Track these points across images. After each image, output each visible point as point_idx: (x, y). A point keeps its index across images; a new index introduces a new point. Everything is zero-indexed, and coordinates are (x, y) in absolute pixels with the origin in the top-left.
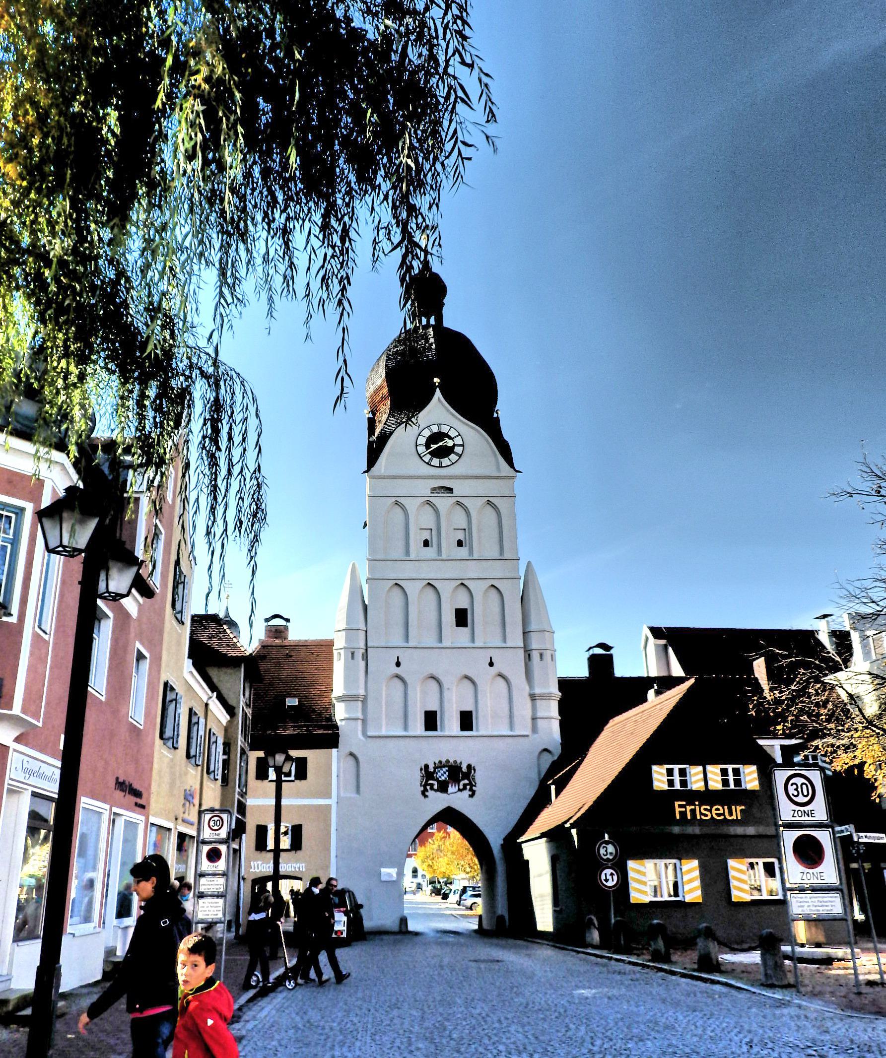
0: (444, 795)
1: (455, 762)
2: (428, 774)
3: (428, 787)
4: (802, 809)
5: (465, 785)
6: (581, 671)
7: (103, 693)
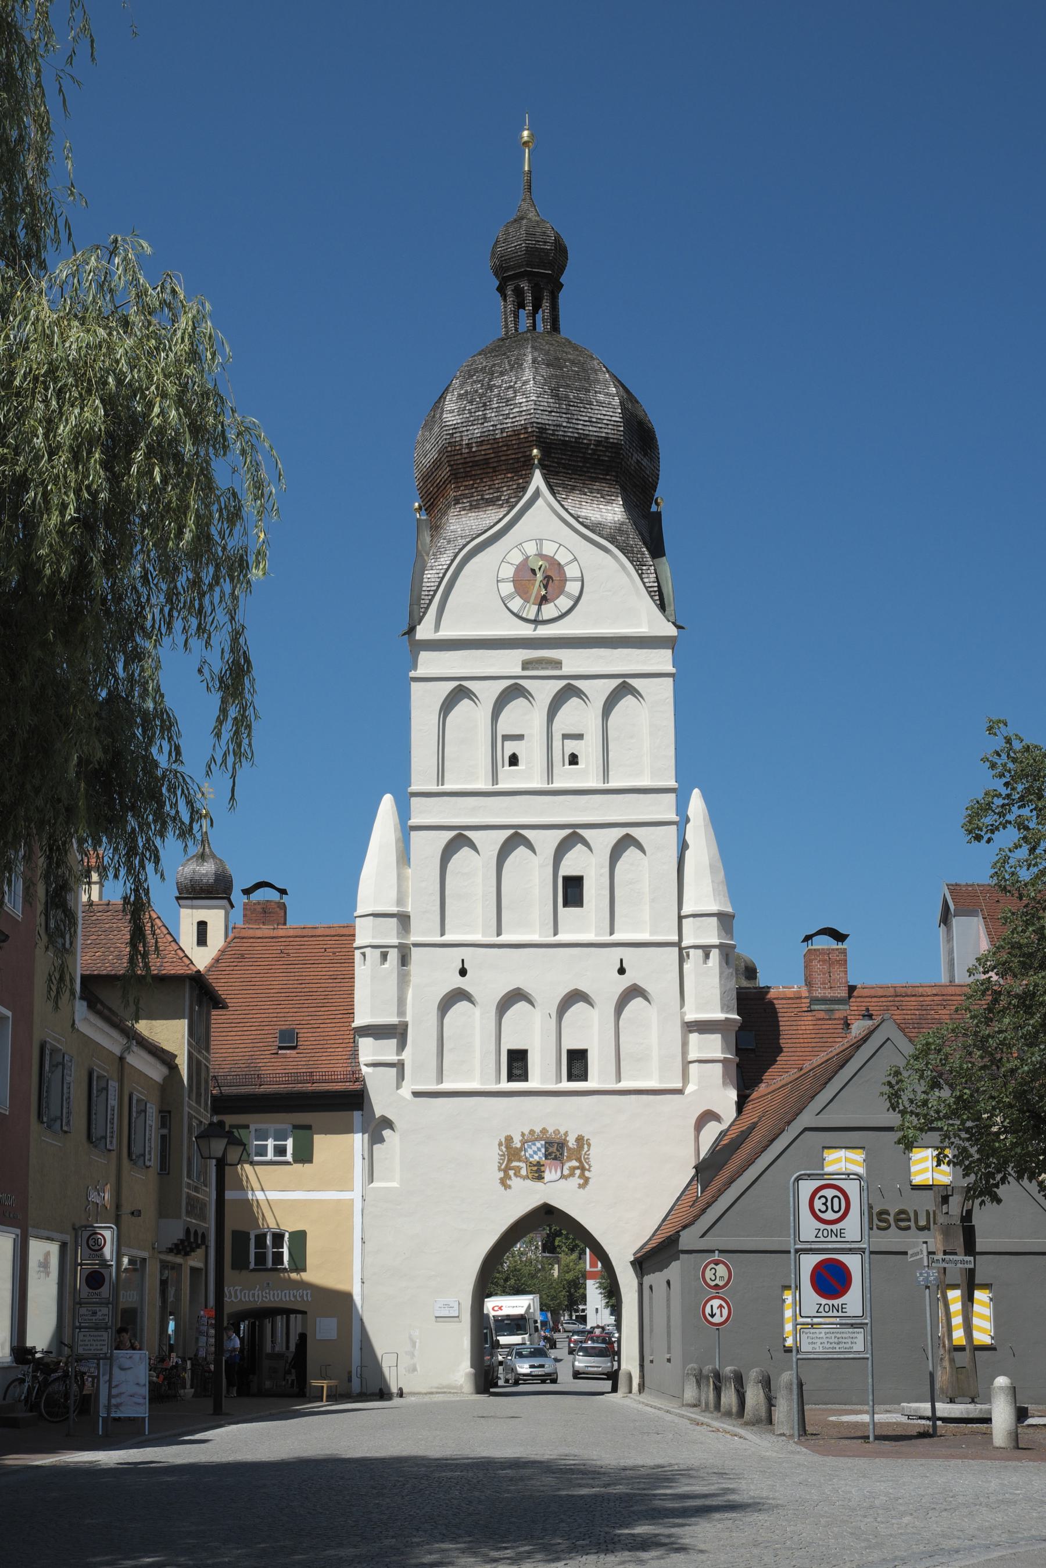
0: (539, 1185)
2: (511, 1153)
3: (511, 1173)
4: (829, 1227)
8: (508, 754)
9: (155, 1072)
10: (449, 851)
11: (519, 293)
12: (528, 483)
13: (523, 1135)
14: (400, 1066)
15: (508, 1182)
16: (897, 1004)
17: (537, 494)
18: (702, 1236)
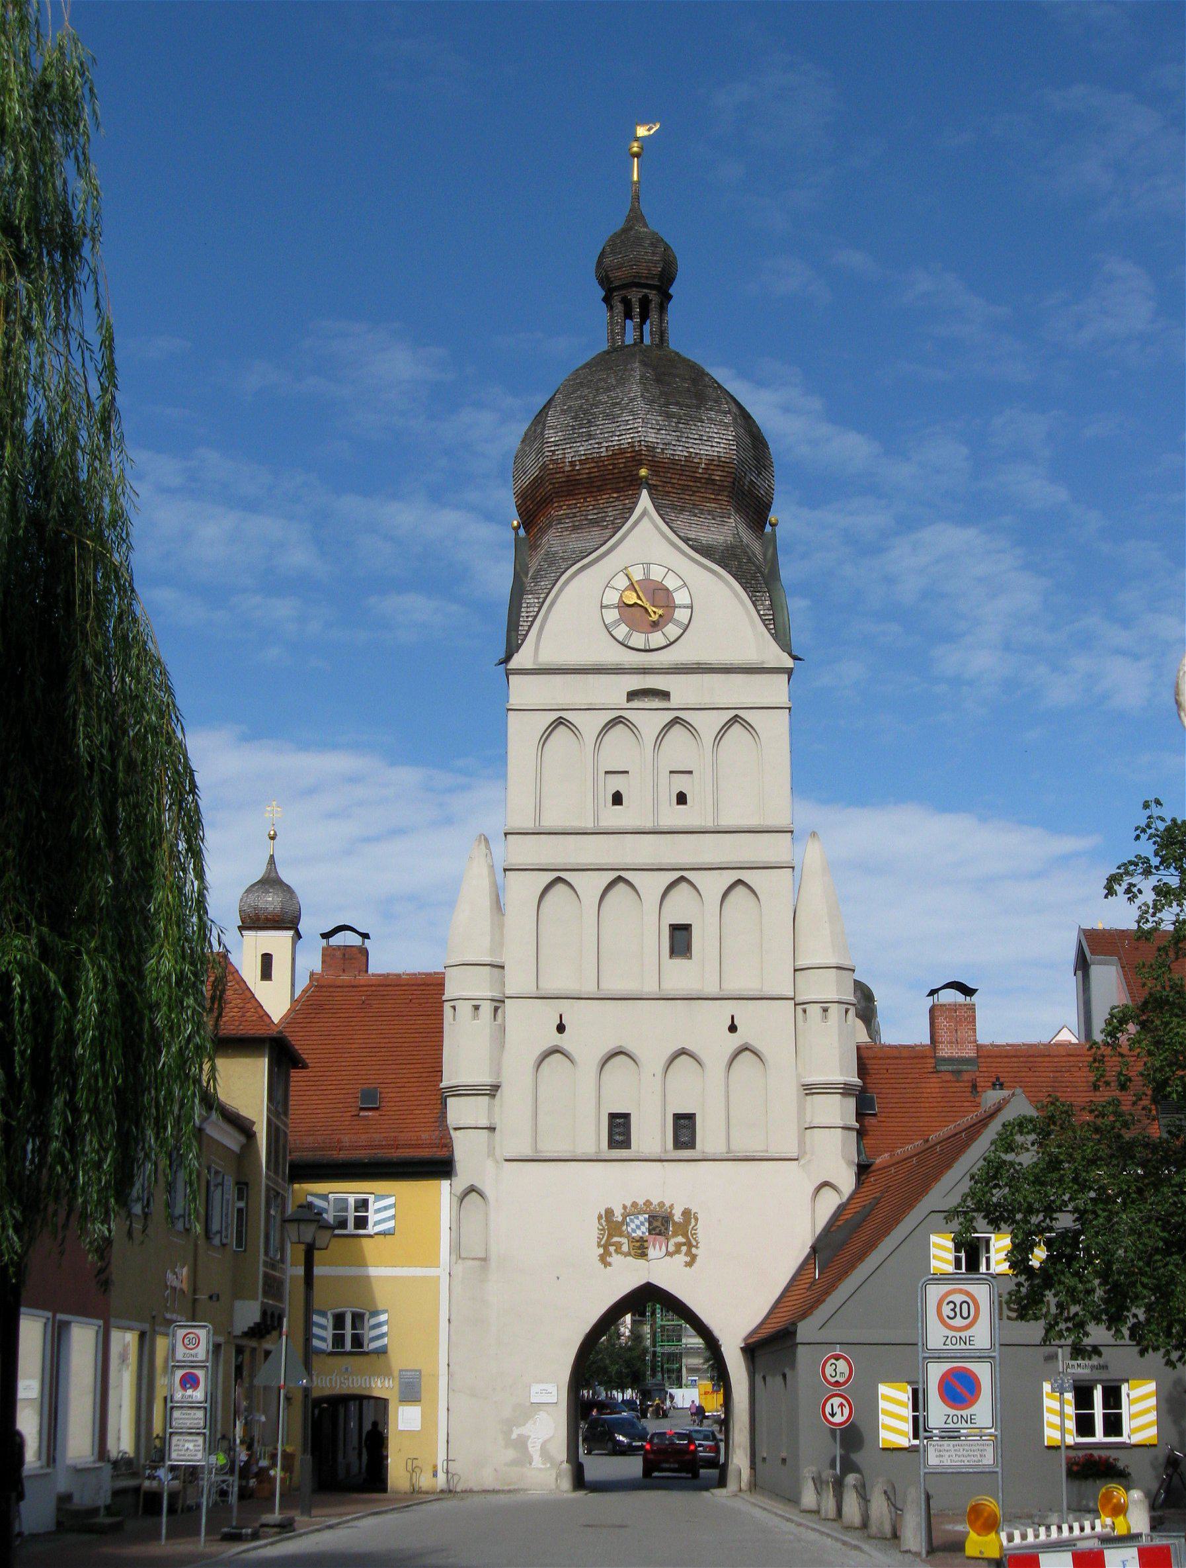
1: (662, 1204)
2: (611, 1226)
3: (612, 1249)
4: (958, 1334)
5: (678, 1246)
9: (231, 1140)
11: (627, 303)
12: (636, 503)
15: (609, 1259)
16: (1030, 1065)
17: (645, 513)
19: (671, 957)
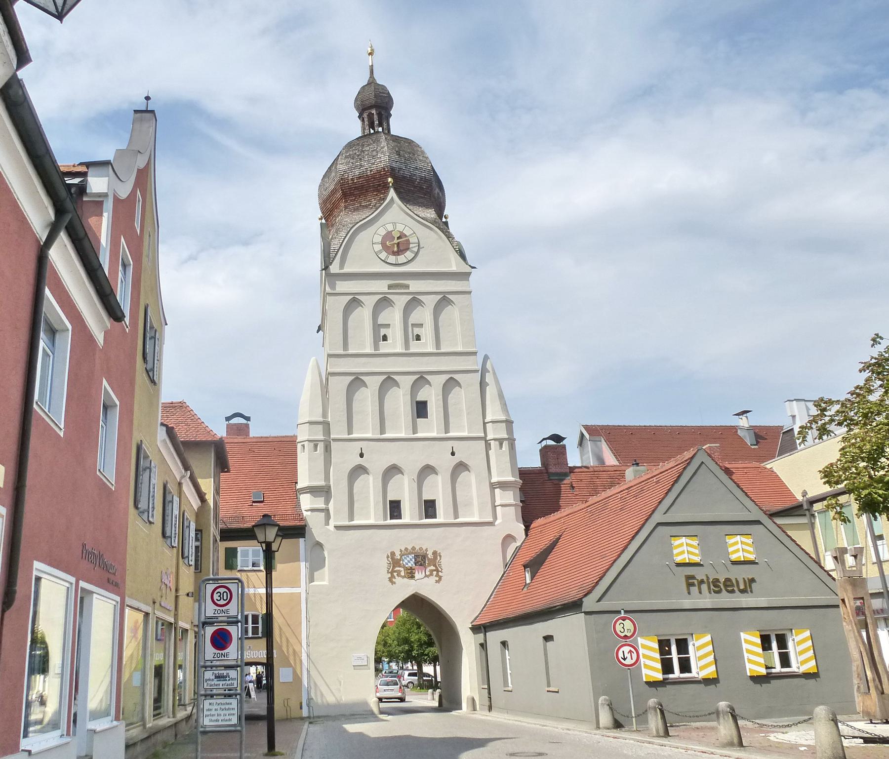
0: (412, 581)
1: (421, 549)
2: (394, 563)
3: (395, 574)
5: (432, 571)
6: (535, 462)
7: (62, 426)
8: (382, 334)
10: (437, 310)
11: (370, 116)
13: (401, 551)
14: (327, 511)
18: (599, 601)
19: (226, 568)
